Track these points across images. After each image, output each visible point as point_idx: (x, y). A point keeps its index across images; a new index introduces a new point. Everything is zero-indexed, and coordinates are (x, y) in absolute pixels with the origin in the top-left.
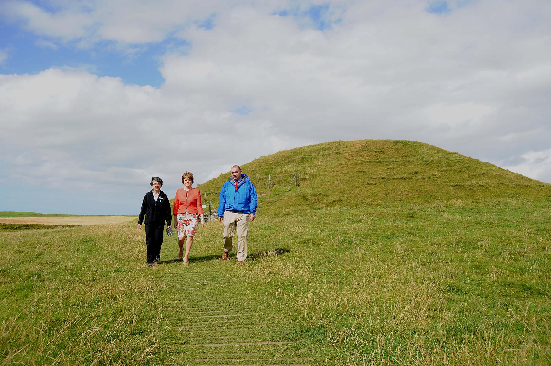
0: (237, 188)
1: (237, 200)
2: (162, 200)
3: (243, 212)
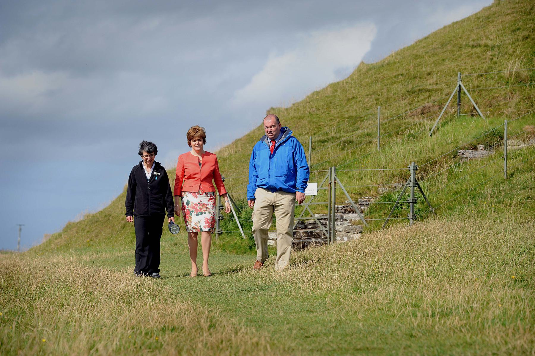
0: (273, 152)
1: (273, 172)
2: (158, 176)
3: (281, 190)
